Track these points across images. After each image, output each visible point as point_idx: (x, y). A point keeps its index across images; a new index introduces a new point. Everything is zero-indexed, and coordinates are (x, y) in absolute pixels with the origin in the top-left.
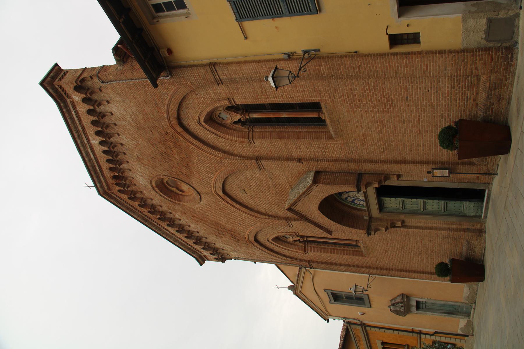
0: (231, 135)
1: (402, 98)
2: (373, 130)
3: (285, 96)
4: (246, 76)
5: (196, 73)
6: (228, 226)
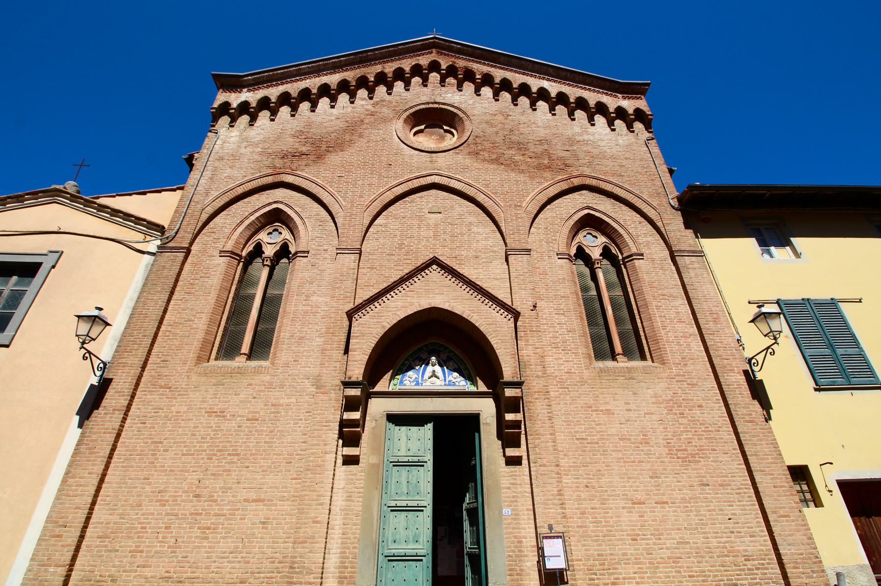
2: (623, 426)
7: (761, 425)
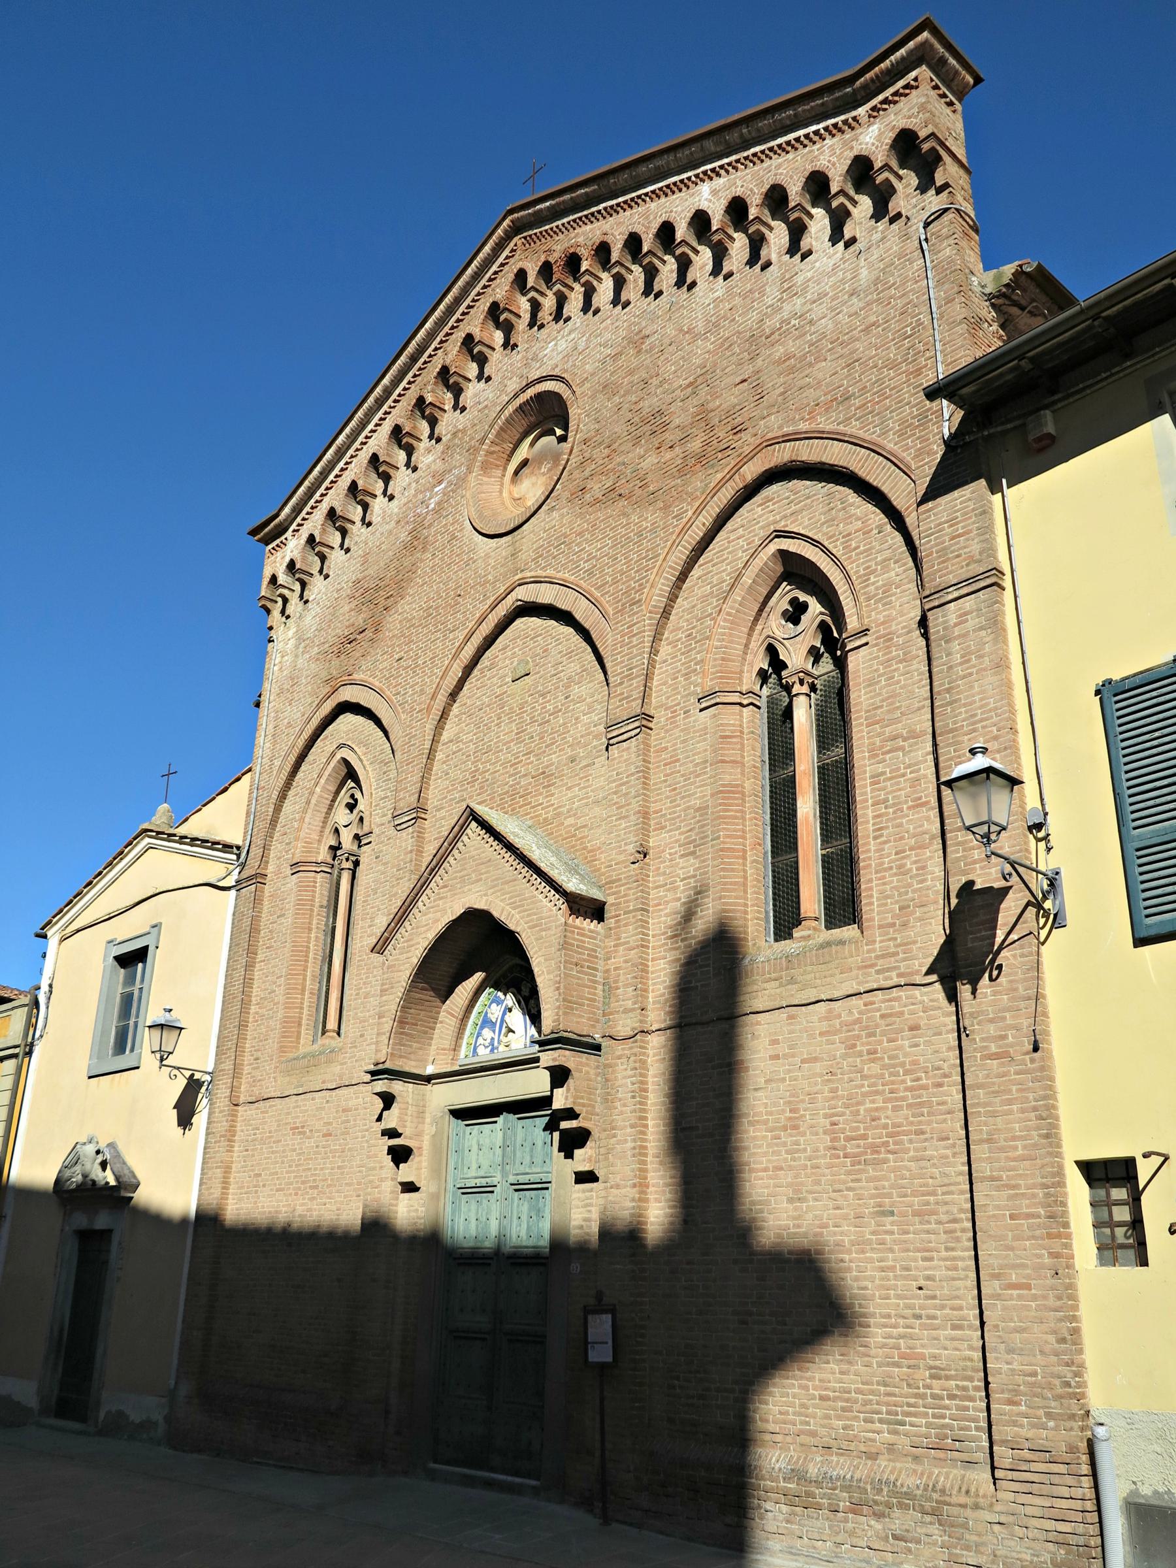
1: (890, 1195)
3: (883, 810)
5: (969, 525)
6: (393, 623)
7: (1023, 1063)
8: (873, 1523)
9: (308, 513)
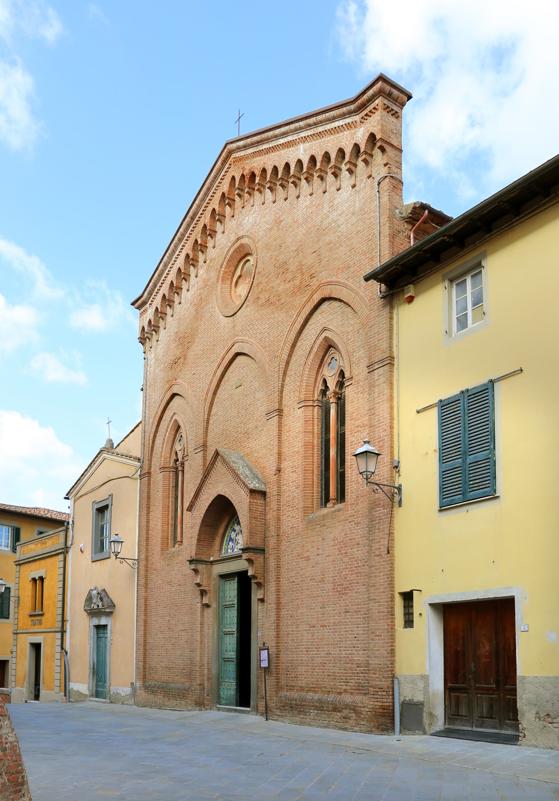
0: (309, 374)
1: (348, 606)
2: (313, 569)
4: (376, 407)
6: (191, 355)
8: (338, 714)
9: (222, 179)
